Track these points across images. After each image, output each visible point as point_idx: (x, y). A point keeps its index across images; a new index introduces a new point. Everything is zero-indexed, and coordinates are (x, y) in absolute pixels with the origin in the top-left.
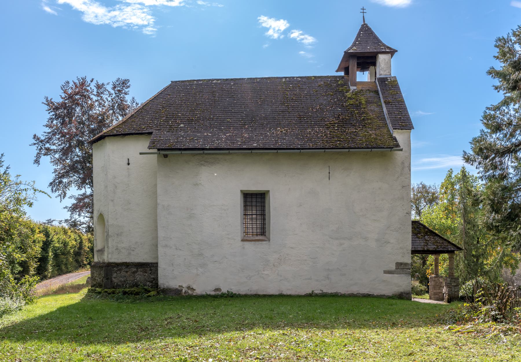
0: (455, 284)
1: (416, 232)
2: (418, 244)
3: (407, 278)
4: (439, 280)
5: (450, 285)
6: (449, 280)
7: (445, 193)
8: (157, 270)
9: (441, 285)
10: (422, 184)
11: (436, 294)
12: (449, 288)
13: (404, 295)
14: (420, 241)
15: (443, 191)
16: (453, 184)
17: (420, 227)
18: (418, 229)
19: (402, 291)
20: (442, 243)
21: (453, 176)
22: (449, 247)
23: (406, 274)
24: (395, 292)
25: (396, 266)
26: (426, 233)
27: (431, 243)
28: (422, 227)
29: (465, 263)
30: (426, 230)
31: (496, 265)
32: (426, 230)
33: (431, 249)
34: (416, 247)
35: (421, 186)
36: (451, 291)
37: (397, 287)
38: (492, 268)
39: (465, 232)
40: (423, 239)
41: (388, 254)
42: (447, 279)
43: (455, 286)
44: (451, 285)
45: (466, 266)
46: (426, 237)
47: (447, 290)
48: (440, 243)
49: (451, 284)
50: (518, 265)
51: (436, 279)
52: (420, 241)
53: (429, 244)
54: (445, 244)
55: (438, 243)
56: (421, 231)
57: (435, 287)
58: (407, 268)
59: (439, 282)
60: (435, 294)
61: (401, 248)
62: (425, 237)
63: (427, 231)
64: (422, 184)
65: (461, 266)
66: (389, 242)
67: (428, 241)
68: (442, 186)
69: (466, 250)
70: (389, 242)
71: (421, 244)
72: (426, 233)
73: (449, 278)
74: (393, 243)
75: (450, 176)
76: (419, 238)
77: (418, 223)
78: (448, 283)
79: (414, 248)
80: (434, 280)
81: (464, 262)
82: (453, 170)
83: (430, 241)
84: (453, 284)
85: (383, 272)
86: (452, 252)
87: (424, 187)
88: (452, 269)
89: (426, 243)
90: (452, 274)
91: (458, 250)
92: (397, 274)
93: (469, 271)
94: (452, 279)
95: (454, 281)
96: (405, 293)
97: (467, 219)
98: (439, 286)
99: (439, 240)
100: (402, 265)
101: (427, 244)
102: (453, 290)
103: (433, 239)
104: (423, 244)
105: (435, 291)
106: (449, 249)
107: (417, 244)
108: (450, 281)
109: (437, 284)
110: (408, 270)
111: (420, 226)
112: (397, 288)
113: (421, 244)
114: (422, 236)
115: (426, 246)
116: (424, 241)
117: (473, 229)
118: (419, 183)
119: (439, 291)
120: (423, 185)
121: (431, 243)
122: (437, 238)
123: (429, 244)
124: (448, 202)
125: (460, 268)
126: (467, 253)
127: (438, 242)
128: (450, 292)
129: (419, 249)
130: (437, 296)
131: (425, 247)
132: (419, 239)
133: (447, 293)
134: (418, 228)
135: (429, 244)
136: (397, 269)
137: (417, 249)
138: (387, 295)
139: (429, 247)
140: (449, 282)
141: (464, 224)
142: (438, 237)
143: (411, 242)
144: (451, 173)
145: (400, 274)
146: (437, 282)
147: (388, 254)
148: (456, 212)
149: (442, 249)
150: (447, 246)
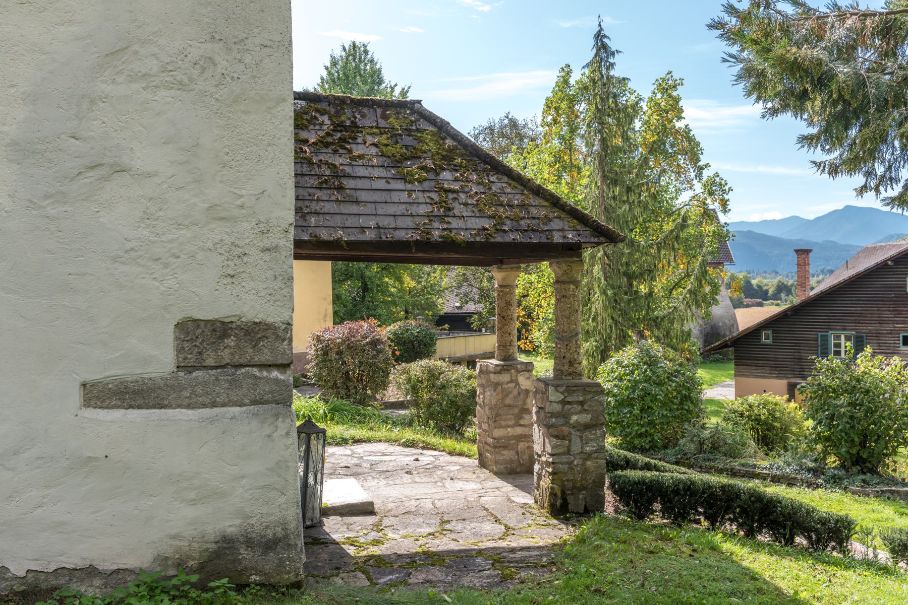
0: (585, 418)
1: (397, 150)
2: (399, 210)
3: (267, 430)
4: (517, 384)
5: (561, 421)
6: (554, 396)
7: (555, 121)
8: (333, 274)
9: (524, 403)
10: (510, 117)
11: (505, 447)
12: (554, 441)
13: (245, 554)
14: (410, 192)
15: (550, 117)
16: (572, 101)
17: (418, 130)
18: (408, 140)
19: (230, 526)
20: (522, 206)
21: (572, 81)
22: (556, 224)
23: (254, 402)
24: (175, 537)
25: (180, 350)
26: (447, 159)
27: (466, 204)
28: (431, 128)
29: (607, 295)
30: (449, 142)
31: (684, 299)
32: (449, 142)
33: (463, 236)
34: (385, 222)
35: (506, 121)
36: (568, 452)
37: (193, 502)
38: (675, 307)
39: (605, 208)
40: (426, 185)
41: (115, 259)
42: (545, 393)
43: (587, 427)
44: (567, 423)
45: (610, 303)
46: (446, 175)
47: (549, 449)
48: (511, 206)
49: (566, 416)
50: (717, 297)
51: (505, 377)
52: (410, 192)
53: (458, 209)
54: (534, 211)
55: (502, 205)
56: (425, 147)
57: (498, 415)
58: (266, 356)
59: (515, 392)
60: (500, 445)
61: (215, 214)
62: (438, 174)
63: (450, 150)
64: (510, 117)
65: (597, 304)
66: (122, 170)
67: (451, 196)
68: (548, 106)
69: (608, 257)
70: (122, 170)
71: (414, 209)
72: (444, 158)
73: (556, 387)
74: (149, 175)
75: (566, 82)
76: (404, 178)
77: (413, 112)
78: (553, 415)
79: (378, 227)
80: (496, 385)
81: (604, 292)
82: (571, 68)
83: (462, 196)
84: (574, 418)
85: (76, 396)
86: (571, 250)
87: (513, 124)
88: (569, 339)
89: (439, 204)
90: (571, 363)
91: (598, 244)
92: (189, 407)
93: (616, 317)
94: (570, 390)
95: (582, 403)
96: (249, 543)
97: (610, 171)
98: (516, 411)
99: (509, 190)
100: (231, 342)
101: (449, 209)
102: (576, 447)
103: (479, 184)
104: (423, 209)
105: (498, 433)
106: (557, 238)
107: (392, 209)
108: (564, 402)
109: (508, 401)
110: (275, 374)
111: (423, 125)
112: (190, 512)
113: (414, 209)
114: (423, 168)
115: (441, 218)
116: (435, 196)
117: (625, 198)
118: (503, 115)
119: (519, 431)
120: (510, 120)
121: (466, 204)
122: (498, 184)
123: (456, 212)
124: (561, 143)
125: (593, 309)
126: (609, 266)
127: (504, 199)
128: (564, 459)
129: (401, 235)
130: (507, 454)
131: (436, 225)
132: (409, 187)
133: (548, 464)
134: (408, 131)
135: (456, 212)
136: (189, 369)
137: (387, 236)
138: (110, 566)
139: (455, 223)
140: (557, 408)
141: (602, 184)
142: (506, 179)
143: (286, 167)
144: (569, 73)
145: (214, 405)
146: (506, 394)
147: (115, 259)
148: (579, 169)
149: (517, 237)
150: (548, 220)
